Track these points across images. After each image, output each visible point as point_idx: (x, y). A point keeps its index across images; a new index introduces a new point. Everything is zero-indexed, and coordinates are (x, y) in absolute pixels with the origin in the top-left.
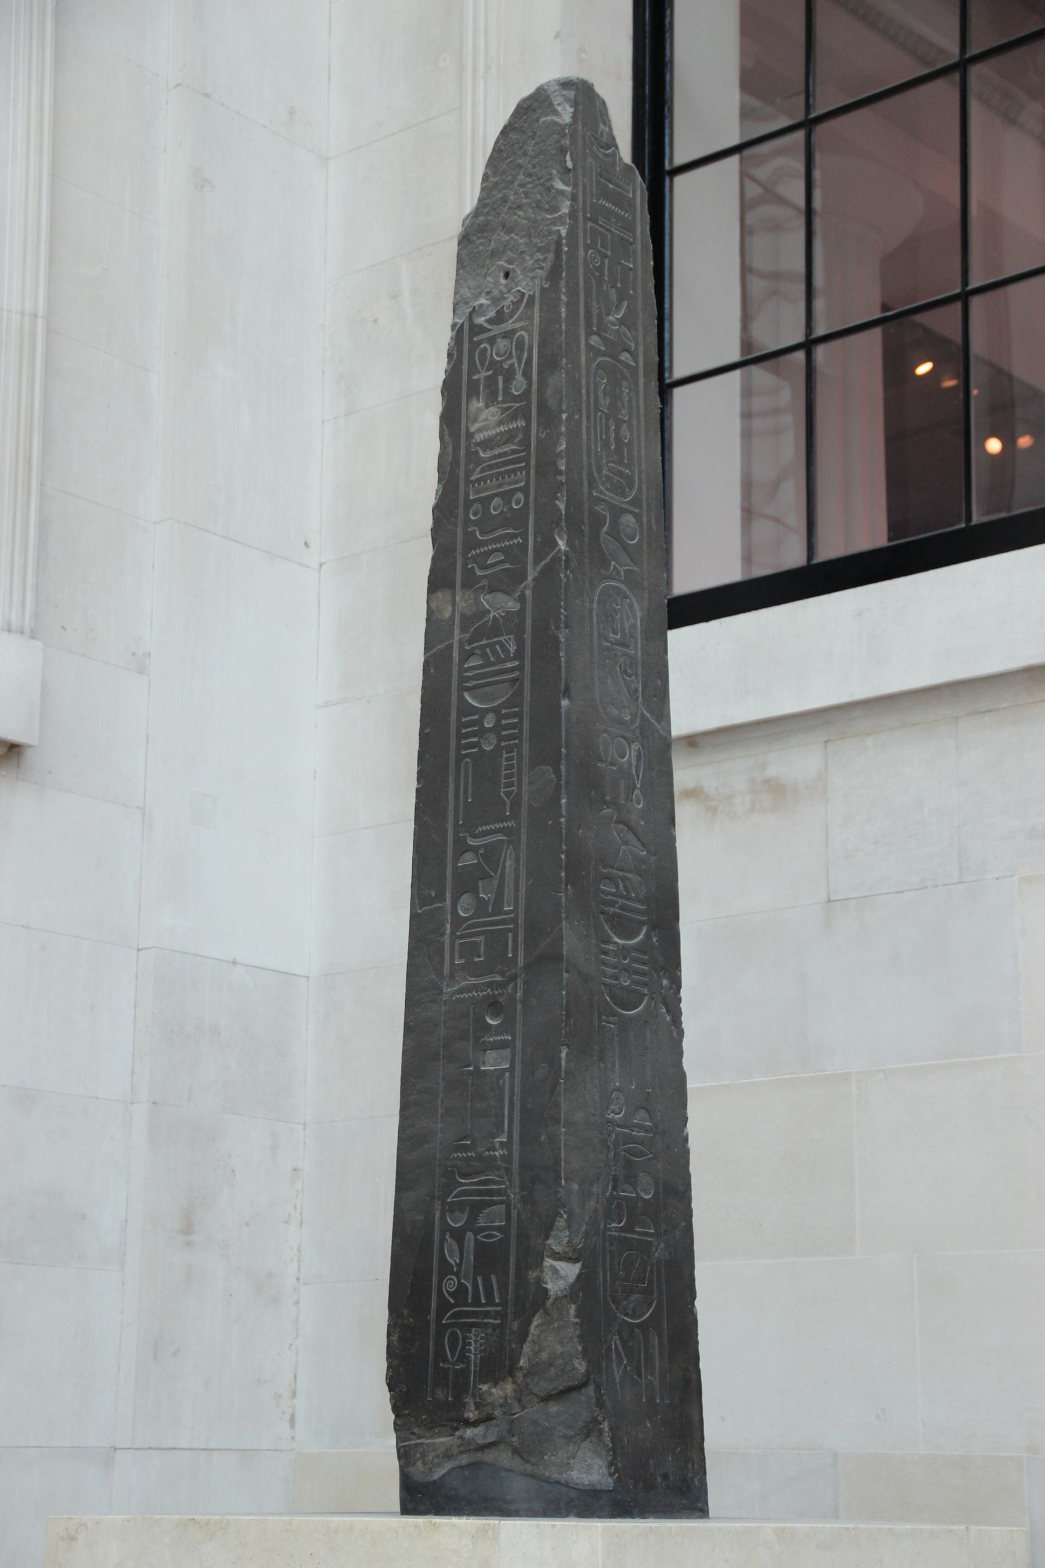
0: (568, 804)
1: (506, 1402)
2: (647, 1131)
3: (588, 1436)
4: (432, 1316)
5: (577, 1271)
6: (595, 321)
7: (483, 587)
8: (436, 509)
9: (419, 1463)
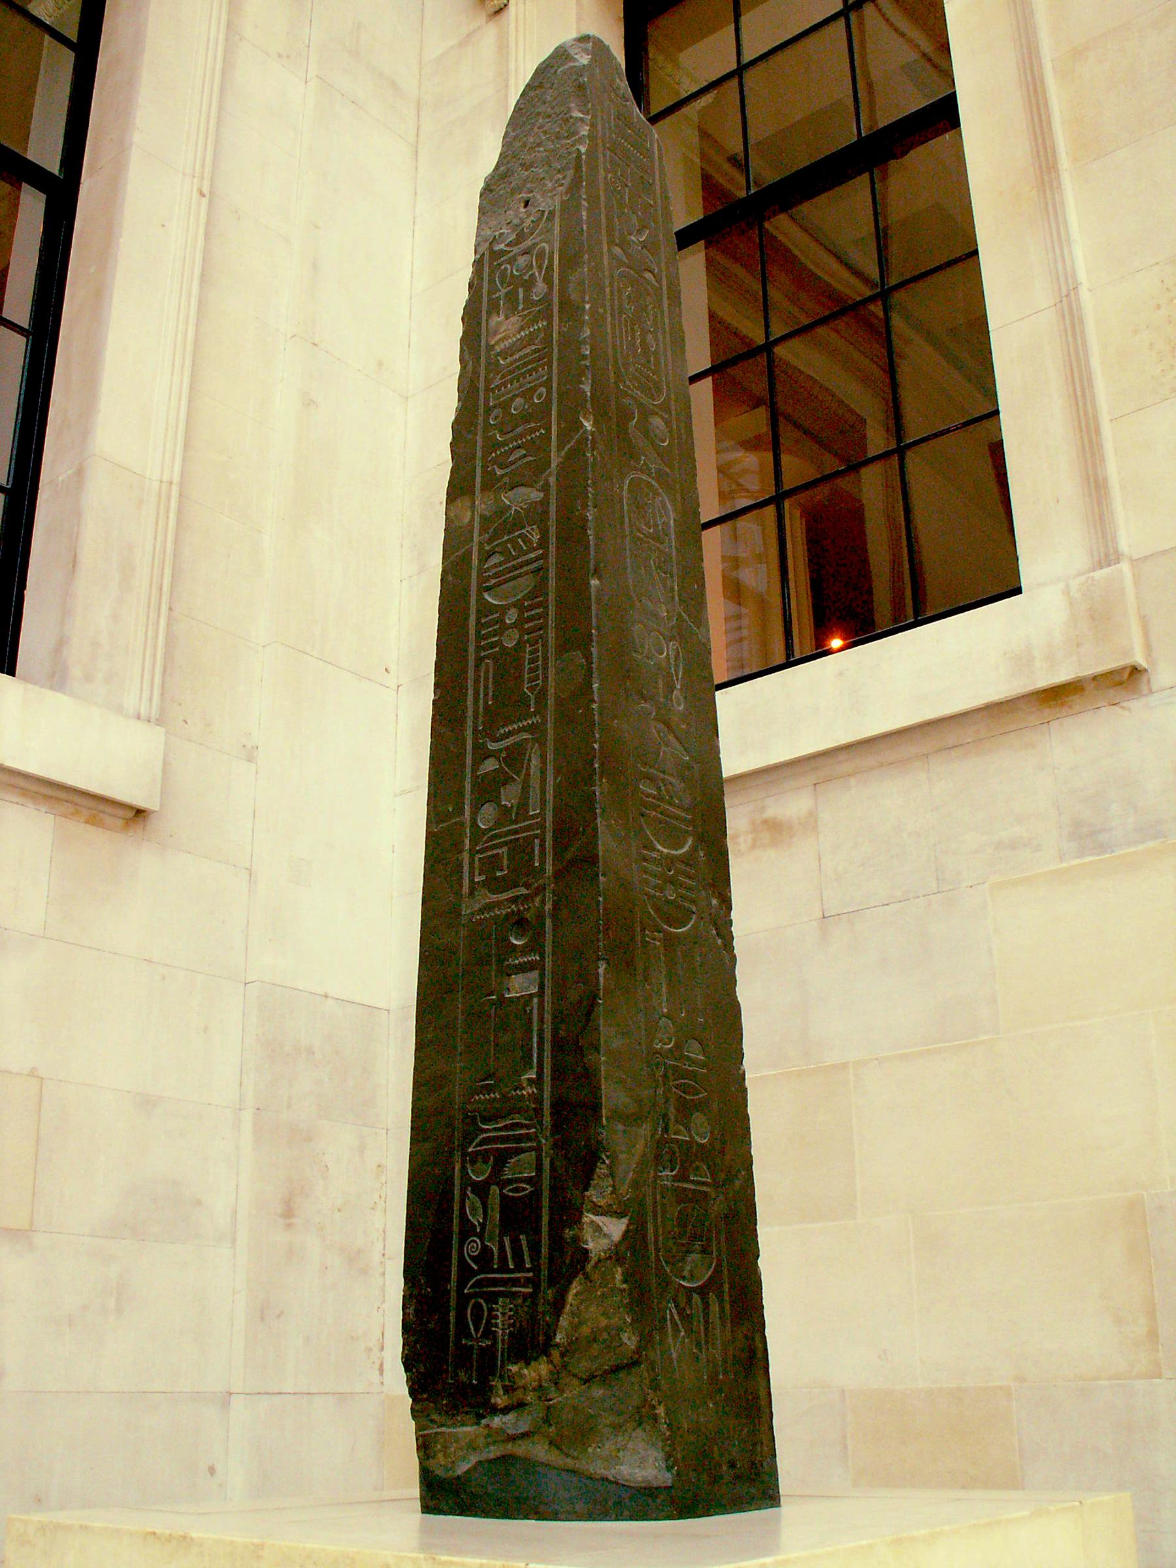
1: (541, 1386)
3: (640, 1424)
5: (624, 1227)
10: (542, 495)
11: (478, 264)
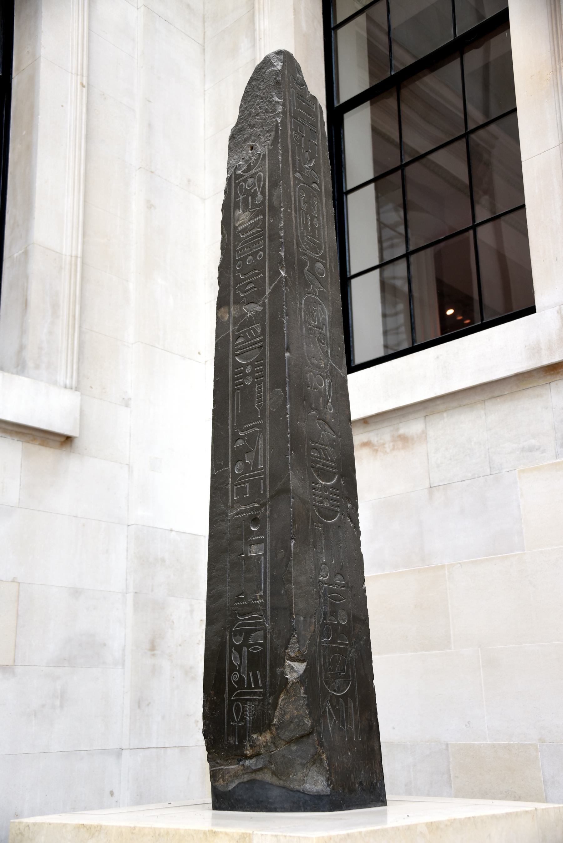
0: (290, 408)
2: (342, 587)
3: (314, 763)
4: (226, 695)
5: (304, 667)
6: (298, 166)
7: (244, 302)
8: (220, 268)
9: (221, 780)
10: (262, 308)
11: (229, 180)
